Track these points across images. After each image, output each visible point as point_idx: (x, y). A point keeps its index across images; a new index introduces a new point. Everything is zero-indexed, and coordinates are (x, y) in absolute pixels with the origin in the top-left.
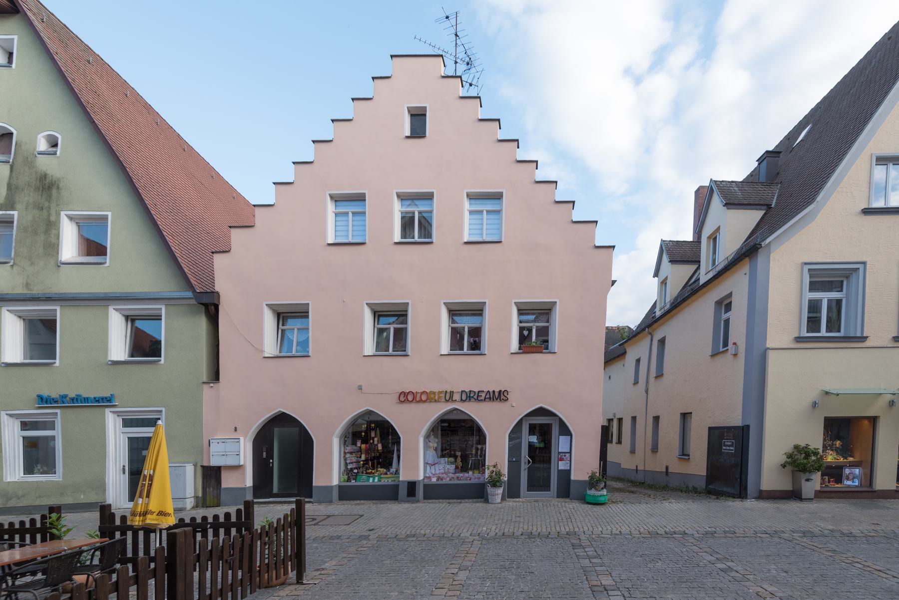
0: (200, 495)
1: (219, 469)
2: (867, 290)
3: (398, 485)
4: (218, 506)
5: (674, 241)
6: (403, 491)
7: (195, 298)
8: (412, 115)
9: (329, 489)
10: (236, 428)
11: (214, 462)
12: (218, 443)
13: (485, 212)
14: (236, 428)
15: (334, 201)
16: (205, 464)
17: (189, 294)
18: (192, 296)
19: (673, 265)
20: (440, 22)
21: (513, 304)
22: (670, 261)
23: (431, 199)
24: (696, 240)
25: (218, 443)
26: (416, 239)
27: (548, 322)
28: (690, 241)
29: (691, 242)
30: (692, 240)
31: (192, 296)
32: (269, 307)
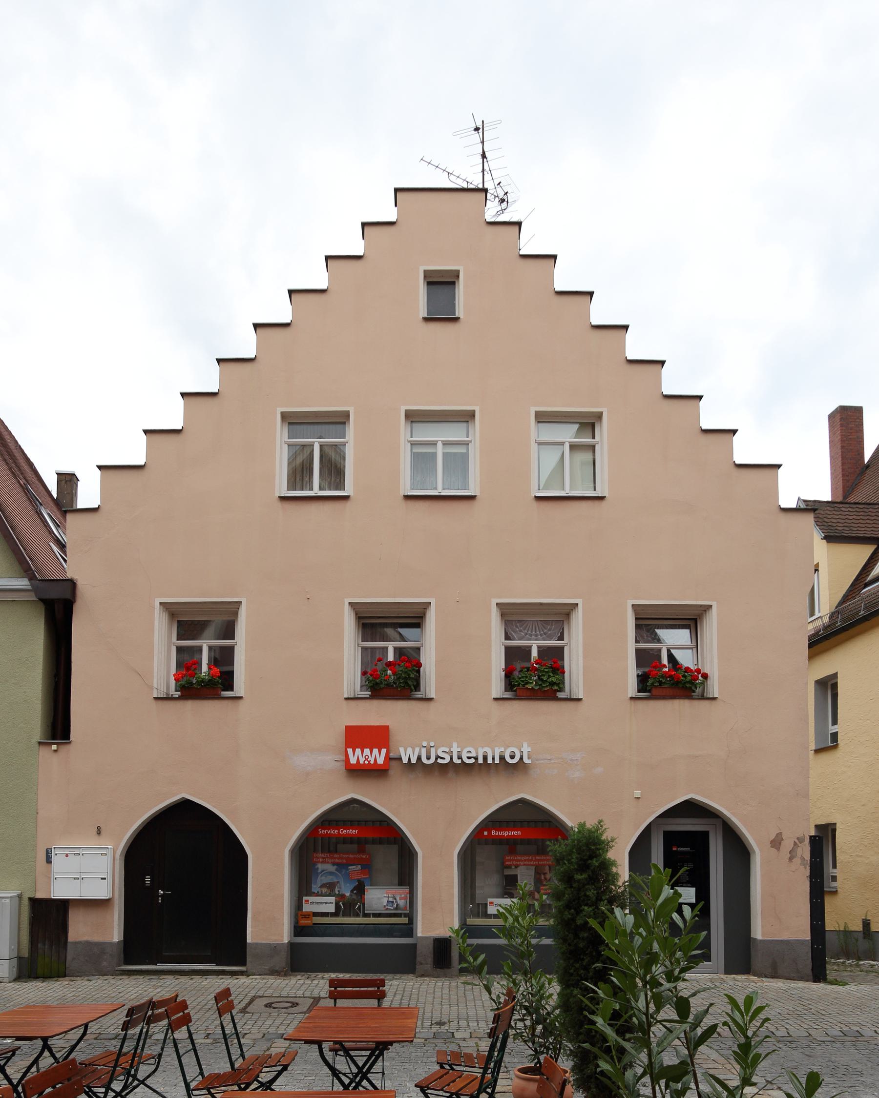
0: (26, 953)
1: (63, 906)
2: (821, 593)
3: (416, 945)
4: (65, 977)
5: (810, 501)
6: (425, 954)
7: (35, 590)
8: (429, 284)
9: (101, 948)
10: (99, 828)
11: (60, 892)
12: (67, 856)
13: (440, 445)
14: (99, 828)
15: (410, 422)
16: (40, 895)
17: (23, 583)
18: (30, 587)
19: (831, 544)
20: (460, 136)
21: (347, 606)
22: (825, 538)
23: (344, 423)
24: (840, 499)
25: (67, 856)
26: (316, 491)
27: (561, 638)
28: (825, 500)
29: (828, 502)
30: (830, 499)
31: (30, 587)
32: (164, 607)
